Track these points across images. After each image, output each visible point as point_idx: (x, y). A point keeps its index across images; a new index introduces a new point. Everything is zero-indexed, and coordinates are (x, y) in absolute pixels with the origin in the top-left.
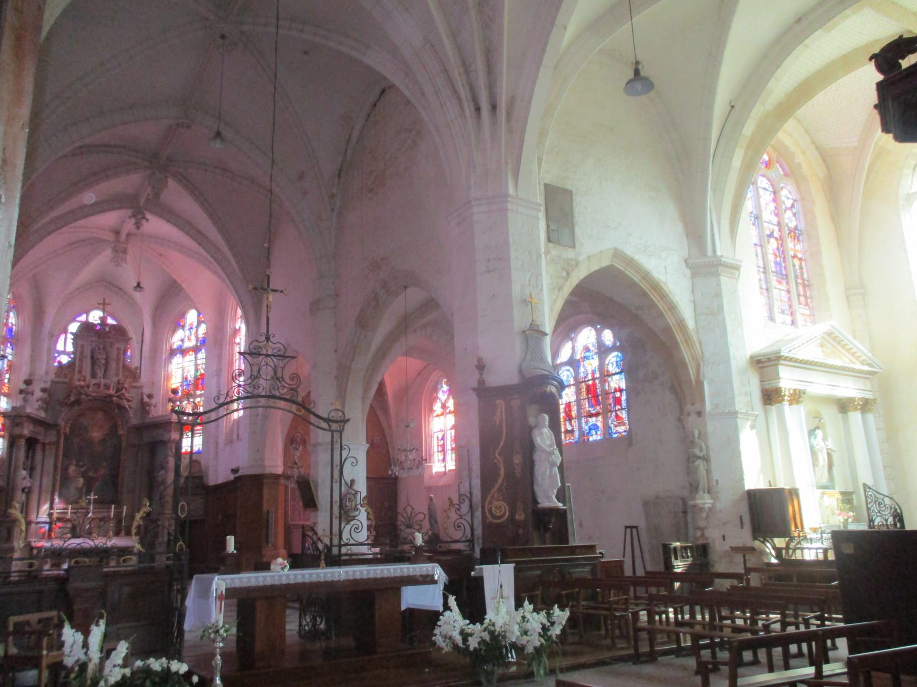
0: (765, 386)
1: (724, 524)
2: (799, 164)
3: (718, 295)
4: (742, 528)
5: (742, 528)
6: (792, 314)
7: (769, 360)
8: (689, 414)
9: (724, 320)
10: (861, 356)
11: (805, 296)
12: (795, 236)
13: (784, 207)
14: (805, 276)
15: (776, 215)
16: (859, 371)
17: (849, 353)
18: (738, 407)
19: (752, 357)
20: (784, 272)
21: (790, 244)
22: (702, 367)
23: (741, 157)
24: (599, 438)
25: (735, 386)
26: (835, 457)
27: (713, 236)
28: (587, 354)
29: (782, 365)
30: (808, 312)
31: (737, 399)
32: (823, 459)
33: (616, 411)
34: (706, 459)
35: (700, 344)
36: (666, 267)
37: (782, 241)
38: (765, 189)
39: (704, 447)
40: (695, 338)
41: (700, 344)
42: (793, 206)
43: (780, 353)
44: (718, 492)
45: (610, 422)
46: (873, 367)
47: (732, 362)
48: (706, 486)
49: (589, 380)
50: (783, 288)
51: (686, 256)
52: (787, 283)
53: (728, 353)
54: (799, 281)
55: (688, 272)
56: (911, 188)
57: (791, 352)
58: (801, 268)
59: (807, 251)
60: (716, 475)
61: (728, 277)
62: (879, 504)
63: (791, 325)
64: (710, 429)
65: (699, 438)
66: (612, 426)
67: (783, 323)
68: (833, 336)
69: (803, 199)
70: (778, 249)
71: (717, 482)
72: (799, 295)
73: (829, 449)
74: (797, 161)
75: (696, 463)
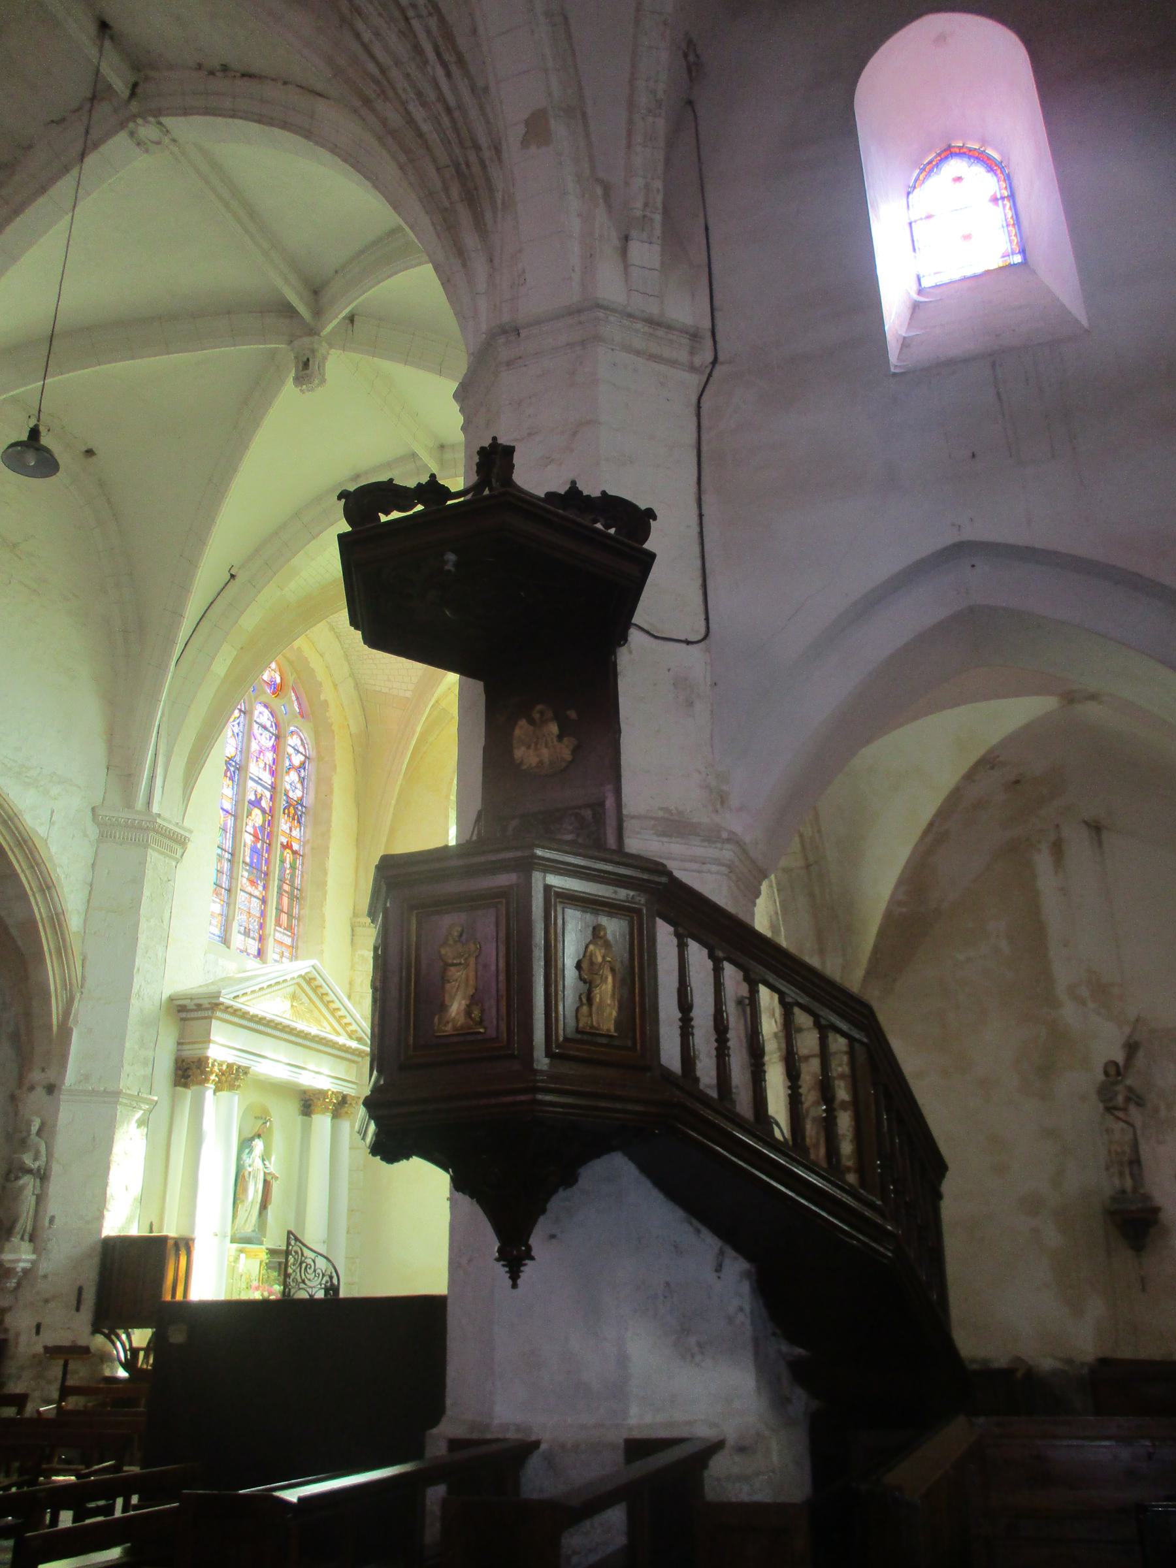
1: (47, 1301)
4: (78, 1309)
5: (78, 1309)
7: (199, 1007)
8: (32, 1088)
11: (290, 915)
12: (296, 813)
13: (287, 763)
14: (298, 881)
15: (273, 773)
19: (171, 999)
20: (264, 868)
21: (284, 824)
26: (276, 1188)
27: (152, 778)
30: (288, 941)
34: (43, 1176)
35: (83, 960)
36: (53, 812)
38: (265, 727)
42: (303, 765)
43: (218, 997)
47: (133, 1001)
48: (29, 1228)
50: (257, 893)
52: (265, 887)
54: (286, 887)
55: (93, 832)
58: (293, 867)
60: (53, 1207)
63: (255, 957)
64: (63, 1117)
65: (39, 1133)
67: (242, 951)
68: (314, 984)
69: (320, 757)
70: (262, 827)
72: (279, 910)
74: (322, 698)
75: (21, 1182)
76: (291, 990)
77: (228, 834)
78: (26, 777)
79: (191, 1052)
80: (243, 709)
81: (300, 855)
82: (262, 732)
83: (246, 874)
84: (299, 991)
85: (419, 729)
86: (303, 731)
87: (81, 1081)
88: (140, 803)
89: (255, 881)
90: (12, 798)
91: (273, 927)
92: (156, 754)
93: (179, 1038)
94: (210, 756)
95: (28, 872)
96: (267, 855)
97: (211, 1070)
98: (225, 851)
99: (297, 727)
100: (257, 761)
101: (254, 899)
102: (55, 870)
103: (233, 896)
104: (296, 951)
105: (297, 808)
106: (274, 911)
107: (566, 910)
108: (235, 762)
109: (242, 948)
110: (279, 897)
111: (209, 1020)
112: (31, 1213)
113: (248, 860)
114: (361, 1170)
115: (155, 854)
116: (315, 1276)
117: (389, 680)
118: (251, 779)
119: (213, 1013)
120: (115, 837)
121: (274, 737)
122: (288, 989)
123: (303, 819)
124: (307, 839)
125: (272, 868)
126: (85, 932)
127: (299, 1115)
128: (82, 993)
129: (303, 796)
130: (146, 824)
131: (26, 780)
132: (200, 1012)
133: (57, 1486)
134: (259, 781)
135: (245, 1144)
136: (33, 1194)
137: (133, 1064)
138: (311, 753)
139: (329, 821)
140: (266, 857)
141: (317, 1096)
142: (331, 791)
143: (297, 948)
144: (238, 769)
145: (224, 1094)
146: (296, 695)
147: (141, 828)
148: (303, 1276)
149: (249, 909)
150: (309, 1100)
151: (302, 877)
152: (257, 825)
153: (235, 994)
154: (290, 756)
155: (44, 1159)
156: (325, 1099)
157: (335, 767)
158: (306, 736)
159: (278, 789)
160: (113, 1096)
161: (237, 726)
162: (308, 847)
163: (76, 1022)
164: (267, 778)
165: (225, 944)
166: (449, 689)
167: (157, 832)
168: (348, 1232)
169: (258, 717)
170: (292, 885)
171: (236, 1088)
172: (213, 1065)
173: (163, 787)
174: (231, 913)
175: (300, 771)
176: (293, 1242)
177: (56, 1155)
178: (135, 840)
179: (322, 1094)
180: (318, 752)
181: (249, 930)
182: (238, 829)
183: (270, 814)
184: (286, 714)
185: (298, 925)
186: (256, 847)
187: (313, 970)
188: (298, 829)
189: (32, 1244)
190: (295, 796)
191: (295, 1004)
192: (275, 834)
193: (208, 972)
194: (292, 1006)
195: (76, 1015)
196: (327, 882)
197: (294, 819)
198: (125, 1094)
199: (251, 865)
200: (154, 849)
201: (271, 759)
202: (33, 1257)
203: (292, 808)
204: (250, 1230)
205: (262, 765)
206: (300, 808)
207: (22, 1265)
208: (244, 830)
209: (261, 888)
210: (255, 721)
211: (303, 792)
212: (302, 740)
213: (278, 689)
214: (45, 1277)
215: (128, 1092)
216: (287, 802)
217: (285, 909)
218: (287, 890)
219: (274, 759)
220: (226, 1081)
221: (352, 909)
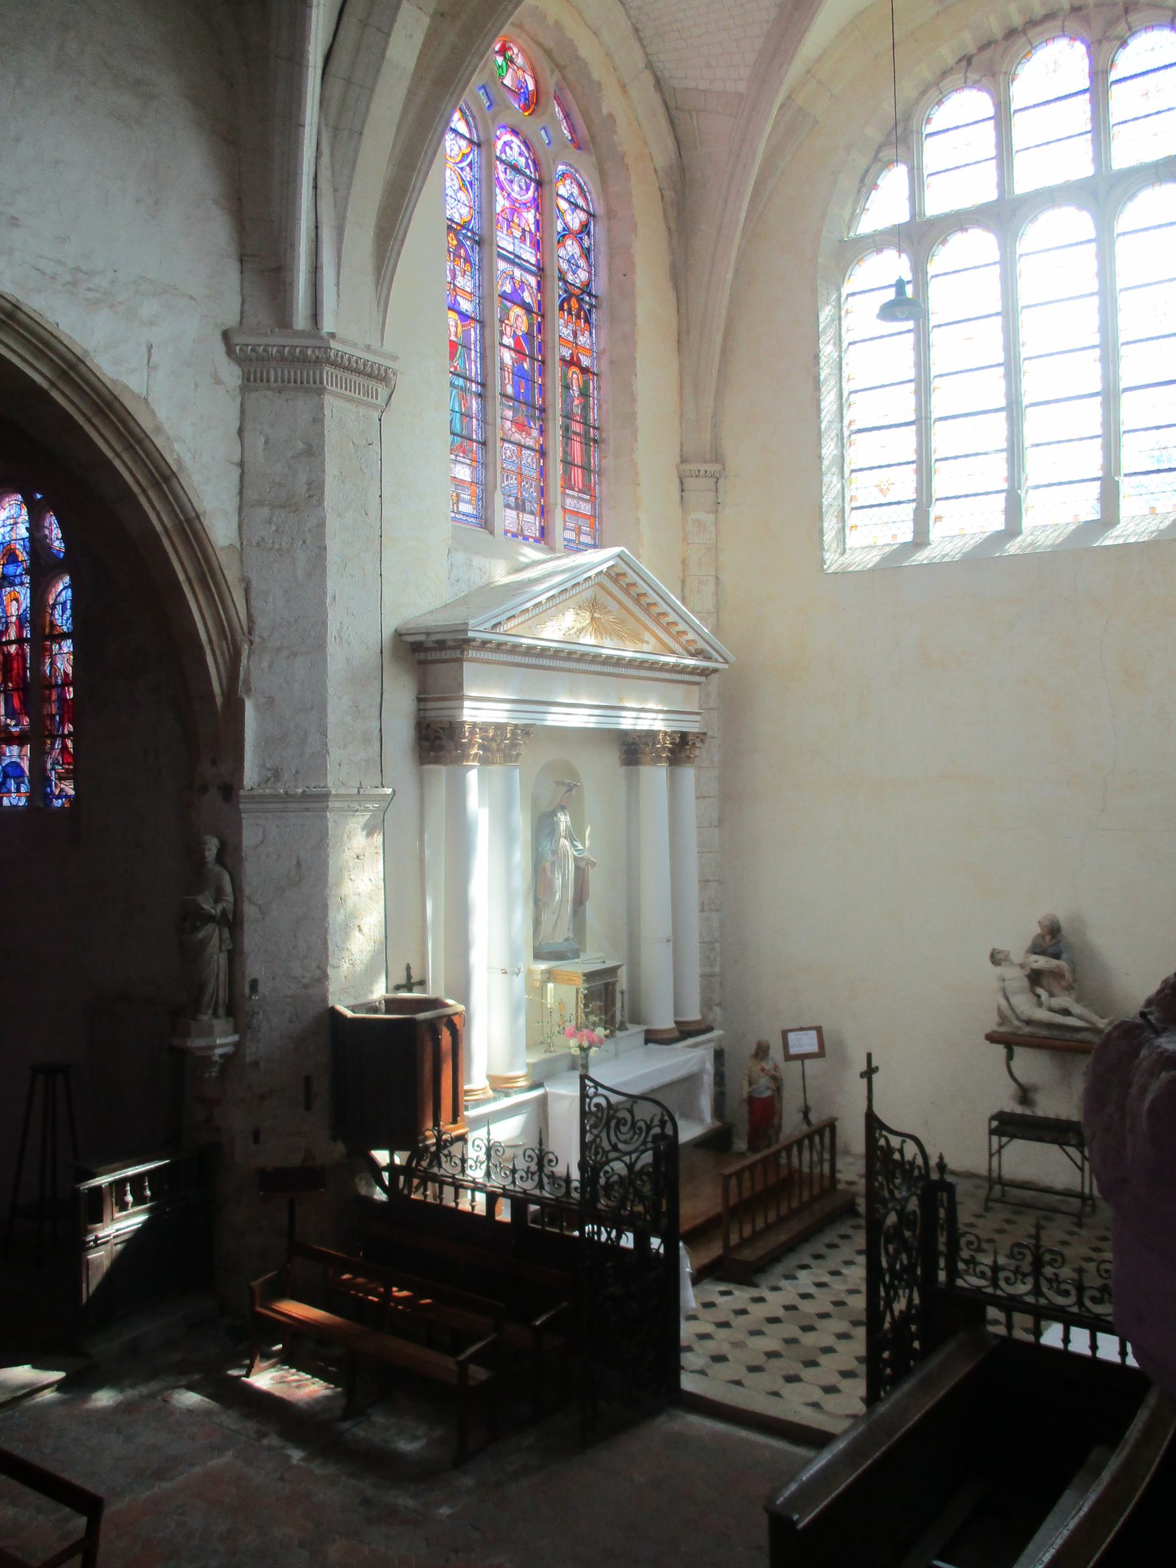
0: (430, 714)
1: (262, 1097)
2: (611, 116)
3: (313, 452)
4: (308, 1107)
5: (308, 1107)
6: (543, 512)
7: (441, 645)
8: (204, 789)
9: (321, 525)
10: (684, 633)
11: (586, 469)
12: (581, 308)
13: (560, 226)
14: (593, 416)
15: (537, 245)
16: (683, 670)
17: (659, 624)
18: (332, 783)
19: (398, 635)
20: (538, 401)
21: (563, 327)
22: (245, 654)
23: (419, 39)
24: (22, 802)
25: (332, 718)
26: (596, 881)
27: (315, 270)
28: (11, 569)
29: (472, 660)
30: (586, 508)
31: (335, 754)
32: (562, 883)
33: (63, 737)
34: (233, 923)
35: (247, 591)
36: (150, 348)
37: (543, 316)
38: (515, 168)
39: (228, 887)
40: (231, 574)
41: (247, 591)
42: (585, 227)
43: (465, 631)
44: (254, 1013)
45: (49, 766)
46: (709, 658)
47: (332, 648)
48: (223, 995)
49: (10, 642)
50: (530, 442)
51: (231, 318)
52: (542, 431)
53: (322, 624)
54: (576, 427)
55: (231, 374)
56: (849, 229)
57: (502, 629)
58: (584, 394)
59: (604, 351)
60: (254, 967)
61: (351, 400)
62: (617, 1127)
63: (537, 540)
64: (249, 837)
65: (220, 859)
66: (53, 776)
67: (515, 535)
68: (623, 582)
69: (611, 215)
70: (529, 335)
71: (254, 984)
72: (568, 463)
73: (582, 859)
74: (605, 111)
75: (201, 935)
76: (588, 594)
77: (473, 352)
78: (89, 289)
79: (439, 713)
80: (475, 139)
81: (594, 374)
82: (512, 177)
83: (509, 414)
84: (603, 597)
85: (762, 146)
86: (582, 172)
87: (268, 779)
88: (301, 320)
89: (526, 423)
90: (67, 331)
91: (559, 490)
92: (317, 227)
93: (420, 693)
94: (412, 222)
95: (126, 457)
96: (540, 379)
97: (470, 741)
98: (471, 381)
99: (571, 166)
100: (509, 227)
101: (526, 452)
102: (172, 450)
103: (490, 453)
104: (600, 523)
105: (582, 299)
106: (560, 466)
107: (1099, 482)
108: (472, 231)
109: (515, 530)
110: (567, 444)
111: (456, 665)
112: (222, 976)
113: (510, 390)
114: (716, 827)
115: (339, 404)
116: (635, 1133)
117: (708, 65)
118: (500, 256)
119: (462, 653)
120: (268, 381)
121: (533, 184)
122: (584, 595)
123: (594, 316)
124: (602, 346)
125: (549, 400)
126: (242, 544)
127: (621, 766)
128: (251, 643)
129: (590, 281)
130: (313, 352)
131: (90, 295)
132: (443, 652)
133: (326, 1311)
134: (517, 260)
135: (543, 826)
136: (220, 950)
137: (345, 746)
138: (598, 207)
139: (633, 316)
140: (540, 382)
141: (643, 740)
142: (632, 267)
143: (600, 517)
144: (479, 243)
145: (496, 769)
146: (563, 110)
147: (304, 360)
148: (614, 1139)
149: (521, 468)
150: (633, 744)
151: (600, 407)
152: (520, 333)
153: (495, 621)
154: (562, 213)
155: (231, 898)
156: (654, 744)
157: (634, 228)
158: (586, 179)
159: (548, 271)
160: (317, 800)
161: (468, 169)
162: (605, 361)
163: (248, 691)
164: (528, 255)
165: (485, 528)
166: (808, 71)
167: (334, 364)
168: (702, 910)
169: (503, 151)
170: (585, 423)
171: (514, 758)
172: (472, 733)
173: (338, 285)
174: (491, 478)
175: (581, 238)
176: (591, 1091)
177: (247, 891)
178: (302, 383)
179: (651, 735)
180: (607, 205)
181: (523, 501)
182: (488, 344)
183: (538, 313)
184: (549, 143)
185: (600, 483)
186: (521, 368)
187: (622, 564)
188: (587, 334)
189: (231, 1019)
190: (578, 281)
191: (596, 615)
192: (550, 345)
193: (458, 581)
194: (593, 618)
195: (247, 682)
196: (636, 413)
197: (578, 317)
198: (337, 796)
199: (514, 399)
200: (332, 393)
201: (532, 220)
202: (236, 1038)
203: (574, 302)
204: (560, 940)
205: (518, 234)
206: (587, 298)
207: (219, 1051)
208: (497, 343)
209: (535, 433)
210: (498, 159)
211: (590, 273)
212: (579, 185)
213: (532, 102)
214: (256, 1064)
215: (342, 791)
216: (566, 291)
217: (578, 461)
218: (578, 431)
219: (537, 223)
220: (498, 750)
221: (678, 451)
